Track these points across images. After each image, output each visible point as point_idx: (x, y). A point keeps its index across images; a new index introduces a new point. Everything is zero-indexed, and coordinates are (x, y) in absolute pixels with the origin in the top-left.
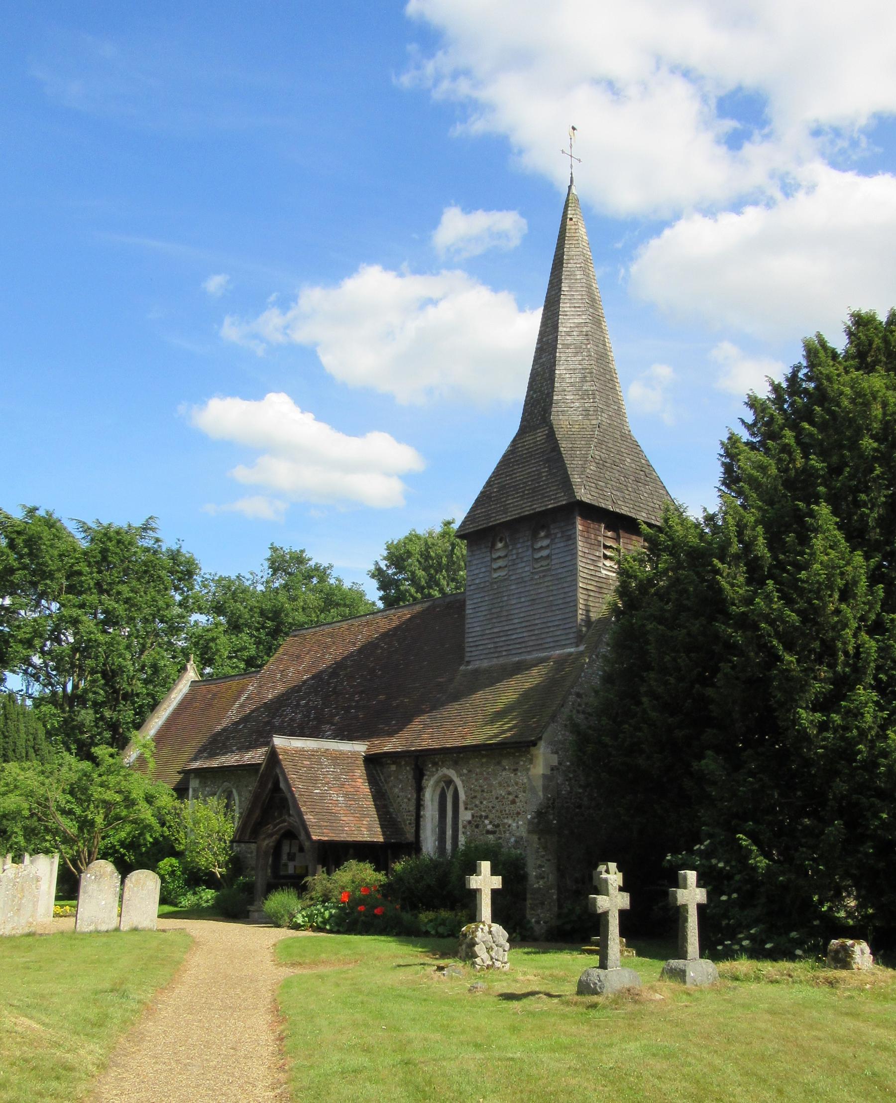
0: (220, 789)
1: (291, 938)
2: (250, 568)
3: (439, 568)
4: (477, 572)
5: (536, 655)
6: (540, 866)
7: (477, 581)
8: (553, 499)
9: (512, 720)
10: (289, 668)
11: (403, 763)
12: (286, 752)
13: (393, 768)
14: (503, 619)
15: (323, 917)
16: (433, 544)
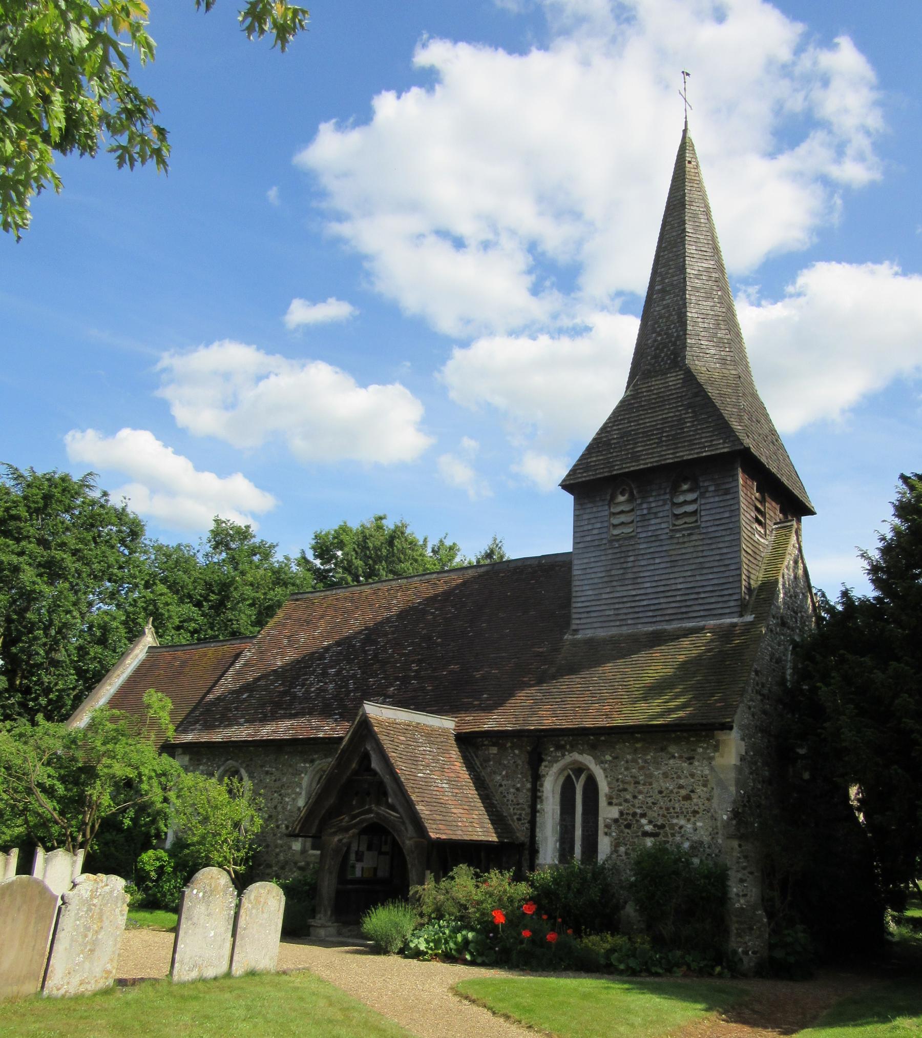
3: (378, 559)
4: (590, 527)
6: (742, 881)
7: (589, 539)
9: (677, 697)
11: (509, 744)
12: (380, 723)
13: (494, 750)
14: (627, 582)
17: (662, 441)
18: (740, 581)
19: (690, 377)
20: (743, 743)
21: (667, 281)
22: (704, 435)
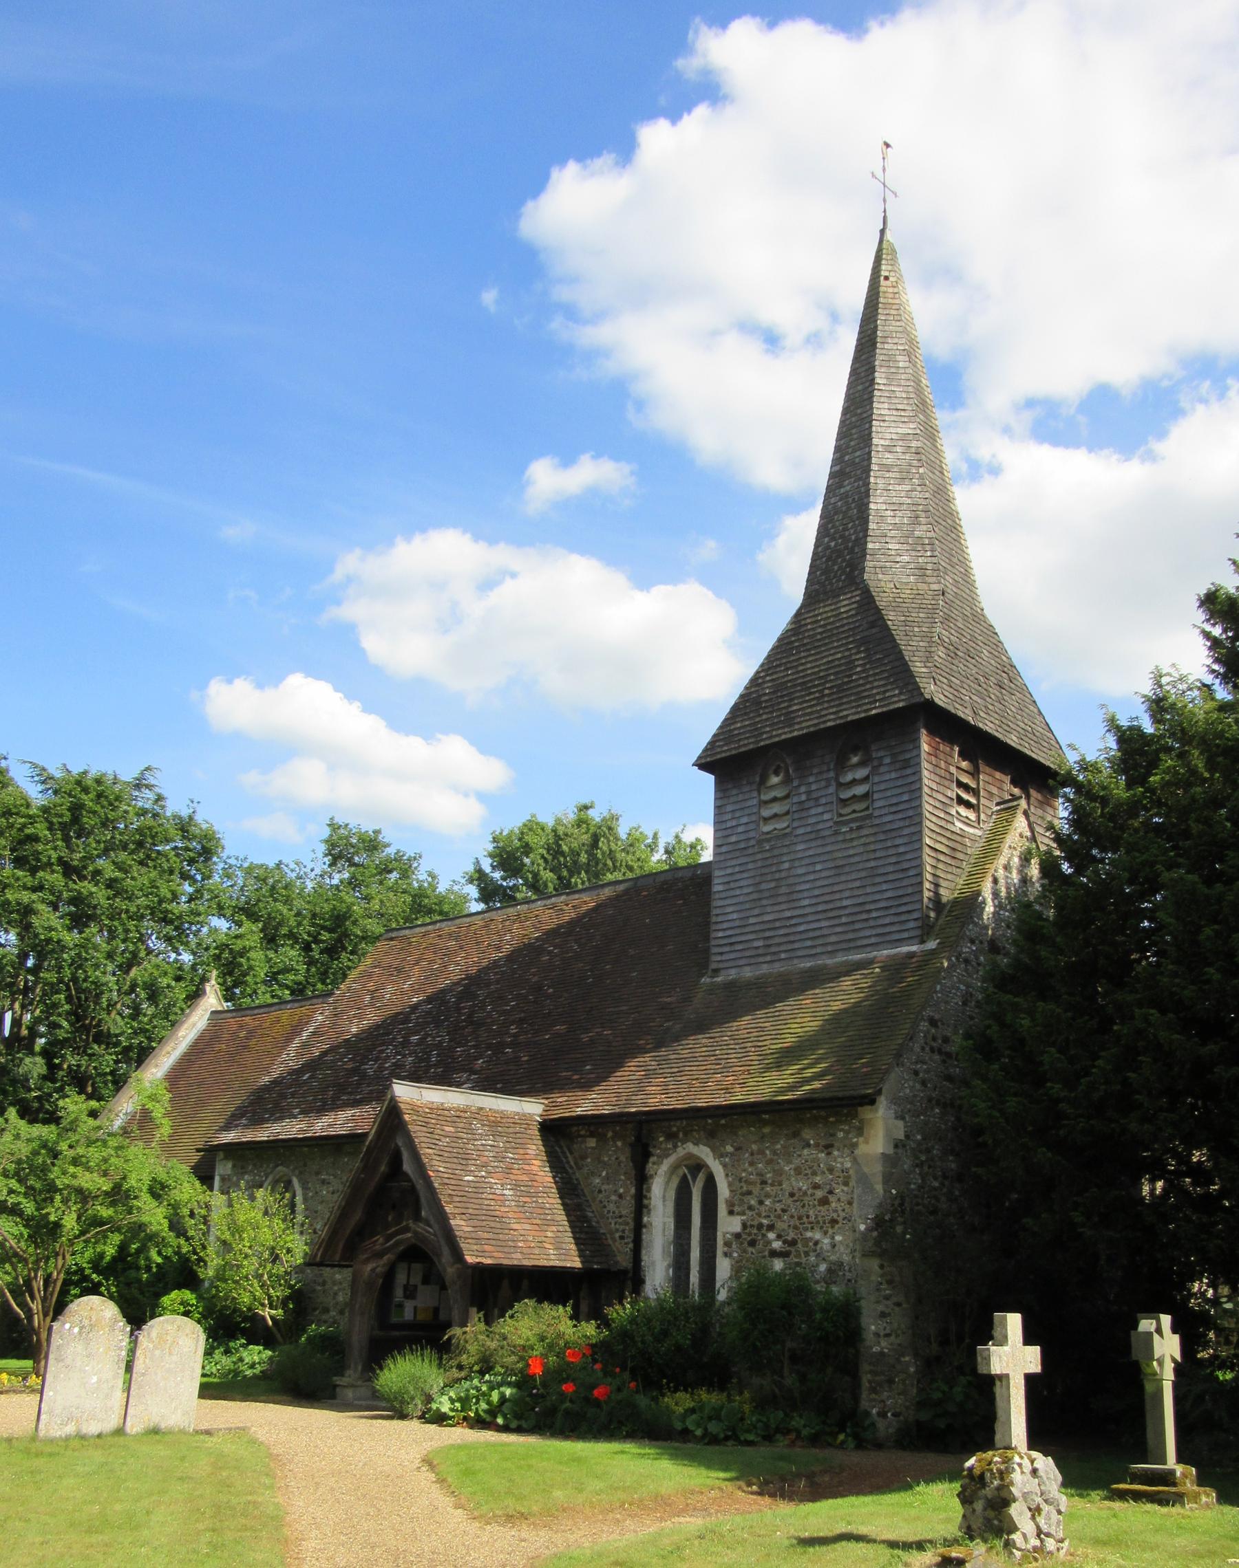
0: (270, 1178)
1: (460, 1447)
2: (299, 853)
3: (575, 869)
4: (734, 823)
5: (841, 958)
6: (883, 1315)
7: (733, 839)
8: (879, 700)
9: (817, 1061)
10: (375, 991)
11: (610, 1134)
12: (415, 1109)
13: (592, 1143)
14: (780, 899)
15: (489, 1403)
16: (566, 835)
17: (824, 696)
18: (921, 892)
19: (868, 602)
20: (900, 1124)
21: (847, 458)
22: (876, 684)
